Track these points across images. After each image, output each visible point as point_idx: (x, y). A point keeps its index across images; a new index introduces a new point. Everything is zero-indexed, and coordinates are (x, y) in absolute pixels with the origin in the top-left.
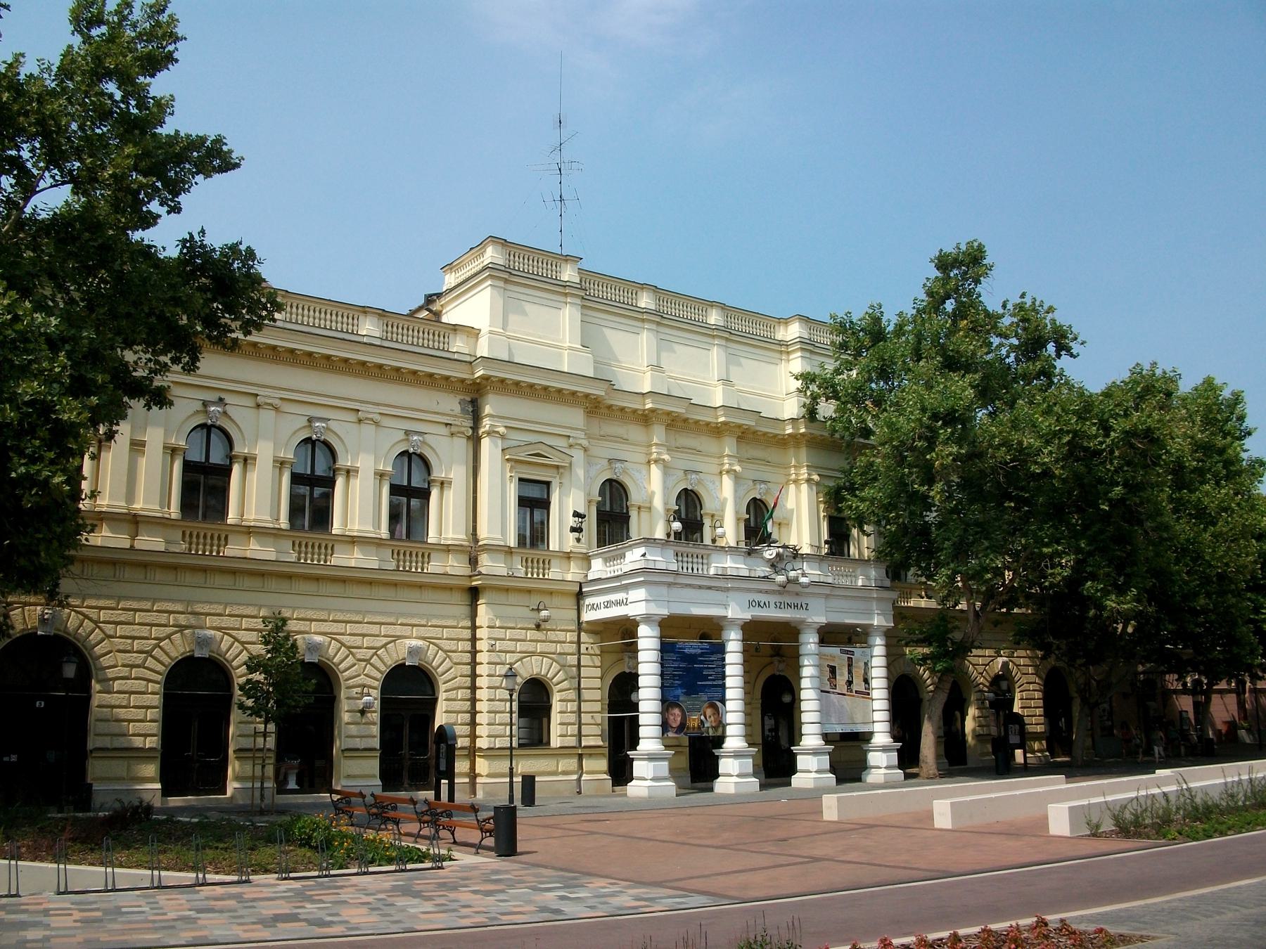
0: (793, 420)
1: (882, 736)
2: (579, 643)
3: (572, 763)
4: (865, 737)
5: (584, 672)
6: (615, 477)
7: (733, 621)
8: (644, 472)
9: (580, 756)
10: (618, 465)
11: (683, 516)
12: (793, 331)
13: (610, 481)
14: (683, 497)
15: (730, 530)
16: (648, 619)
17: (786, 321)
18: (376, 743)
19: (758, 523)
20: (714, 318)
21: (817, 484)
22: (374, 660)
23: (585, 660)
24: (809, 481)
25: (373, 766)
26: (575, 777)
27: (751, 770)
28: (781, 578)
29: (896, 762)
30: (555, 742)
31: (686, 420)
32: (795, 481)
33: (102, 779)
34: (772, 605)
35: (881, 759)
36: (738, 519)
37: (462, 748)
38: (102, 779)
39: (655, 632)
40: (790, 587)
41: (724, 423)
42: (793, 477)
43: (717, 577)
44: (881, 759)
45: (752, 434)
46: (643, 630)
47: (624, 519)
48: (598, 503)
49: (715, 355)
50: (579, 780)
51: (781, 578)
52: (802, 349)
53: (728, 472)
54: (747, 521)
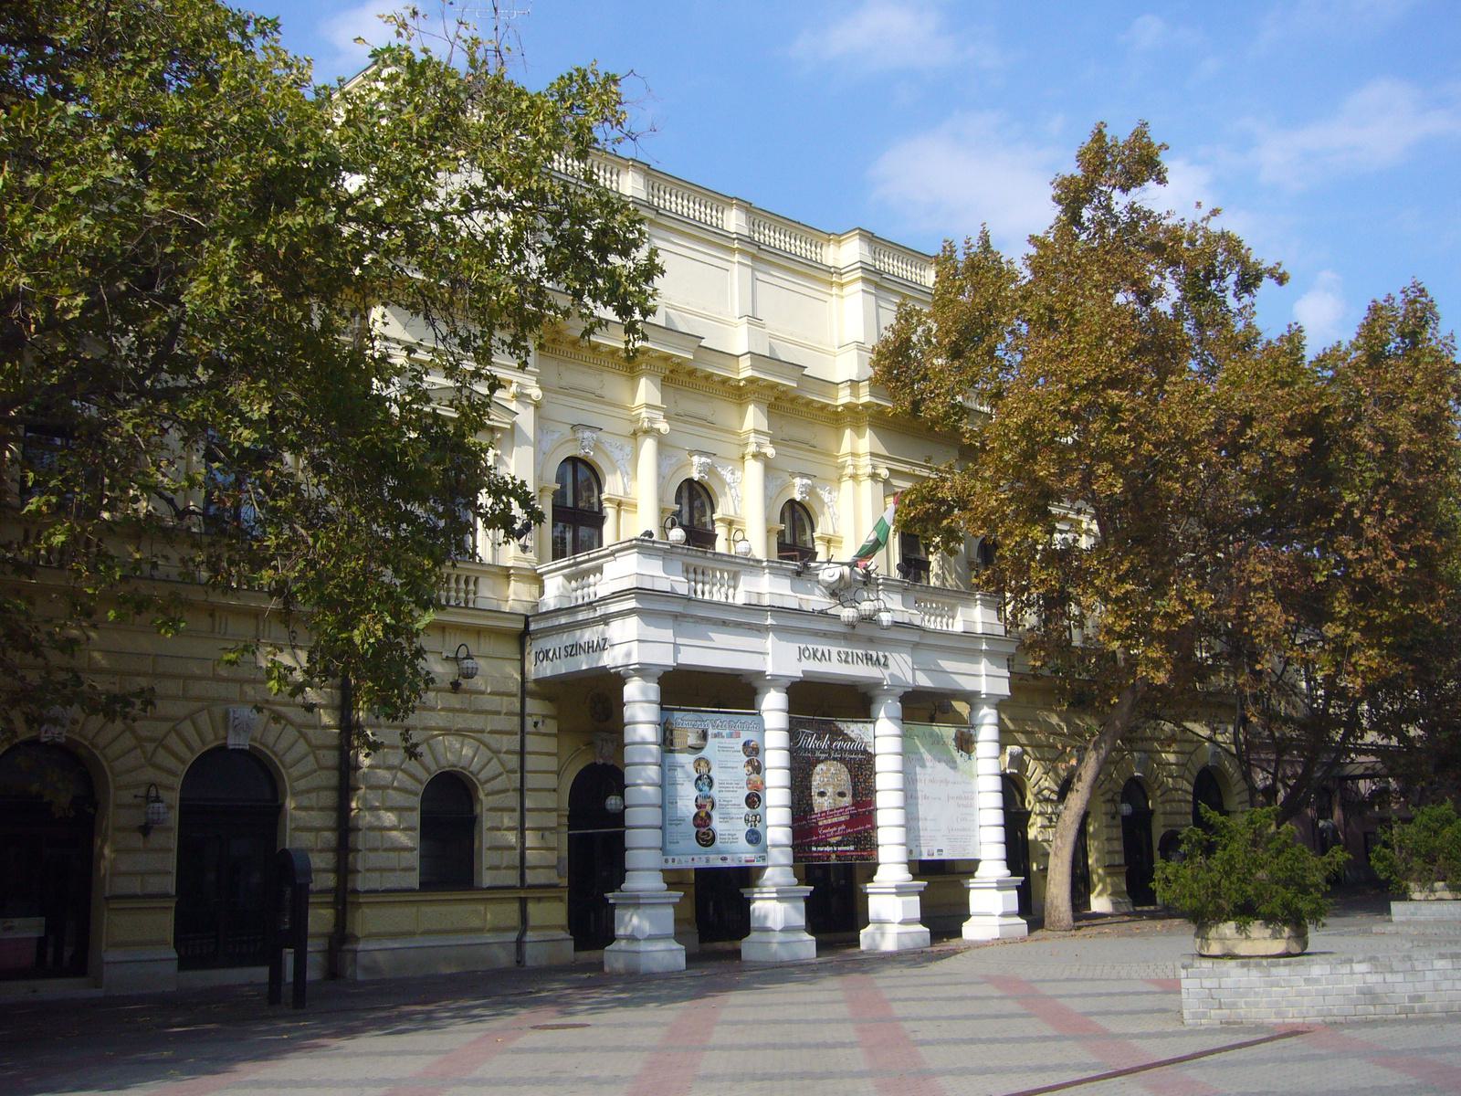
0: (854, 384)
1: (992, 865)
2: (522, 715)
3: (509, 913)
4: (969, 867)
5: (531, 762)
6: (580, 453)
7: (775, 681)
8: (628, 449)
9: (523, 902)
10: (587, 434)
11: (685, 522)
12: (849, 253)
13: (573, 461)
14: (685, 494)
15: (756, 540)
16: (643, 671)
17: (837, 237)
18: (170, 884)
19: (794, 536)
20: (734, 221)
21: (886, 482)
22: (173, 741)
23: (532, 743)
24: (874, 476)
25: (164, 924)
26: (513, 936)
27: (670, 929)
28: (847, 613)
29: (1015, 907)
30: (487, 879)
31: (692, 373)
32: (854, 477)
33: (370, 936)
34: (834, 656)
35: (990, 907)
36: (769, 531)
37: (321, 892)
38: (370, 936)
39: (653, 690)
40: (863, 630)
41: (751, 381)
42: (849, 470)
43: (748, 607)
44: (990, 907)
45: (793, 404)
46: (632, 690)
47: (596, 519)
48: (555, 493)
49: (737, 272)
50: (520, 943)
51: (847, 613)
52: (864, 280)
53: (755, 456)
54: (781, 534)
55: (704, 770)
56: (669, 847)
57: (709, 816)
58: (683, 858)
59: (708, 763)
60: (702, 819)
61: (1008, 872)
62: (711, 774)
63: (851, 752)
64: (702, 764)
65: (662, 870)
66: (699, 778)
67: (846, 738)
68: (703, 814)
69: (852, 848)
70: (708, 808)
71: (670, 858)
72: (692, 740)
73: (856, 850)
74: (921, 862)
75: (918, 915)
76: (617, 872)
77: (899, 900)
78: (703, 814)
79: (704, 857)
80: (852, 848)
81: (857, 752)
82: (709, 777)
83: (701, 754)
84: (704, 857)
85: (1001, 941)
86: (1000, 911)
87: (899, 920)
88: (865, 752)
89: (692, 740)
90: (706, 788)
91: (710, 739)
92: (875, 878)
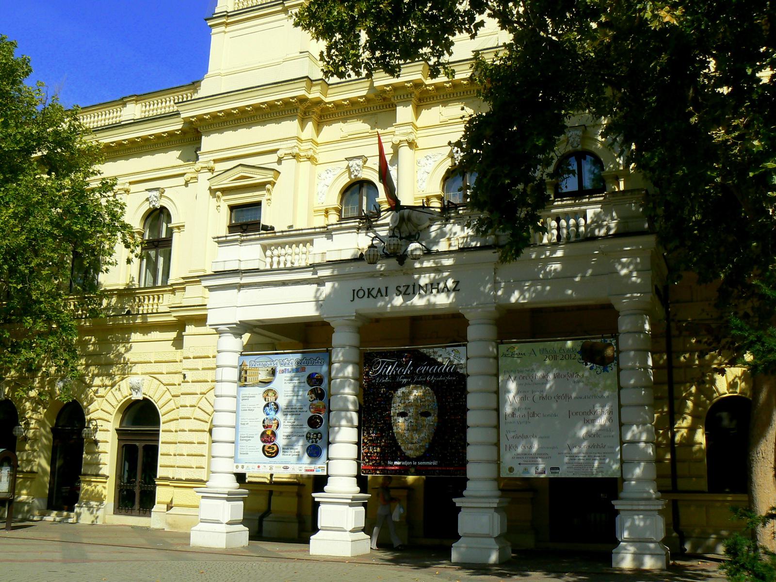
55: (271, 398)
56: (240, 457)
57: (274, 434)
58: (251, 465)
59: (275, 393)
60: (268, 436)
61: (358, 489)
62: (278, 401)
63: (437, 375)
64: (270, 394)
65: (236, 474)
66: (267, 405)
67: (433, 362)
68: (269, 433)
69: (435, 463)
70: (274, 428)
71: (240, 465)
72: (263, 376)
73: (439, 465)
74: (529, 485)
75: (241, 517)
76: (460, 484)
77: (228, 505)
78: (269, 433)
79: (268, 466)
80: (435, 463)
81: (445, 374)
82: (275, 404)
83: (271, 386)
84: (268, 466)
85: (229, 553)
86: (227, 519)
87: (227, 521)
88: (455, 373)
89: (263, 376)
90: (273, 413)
91: (278, 375)
92: (326, 488)
